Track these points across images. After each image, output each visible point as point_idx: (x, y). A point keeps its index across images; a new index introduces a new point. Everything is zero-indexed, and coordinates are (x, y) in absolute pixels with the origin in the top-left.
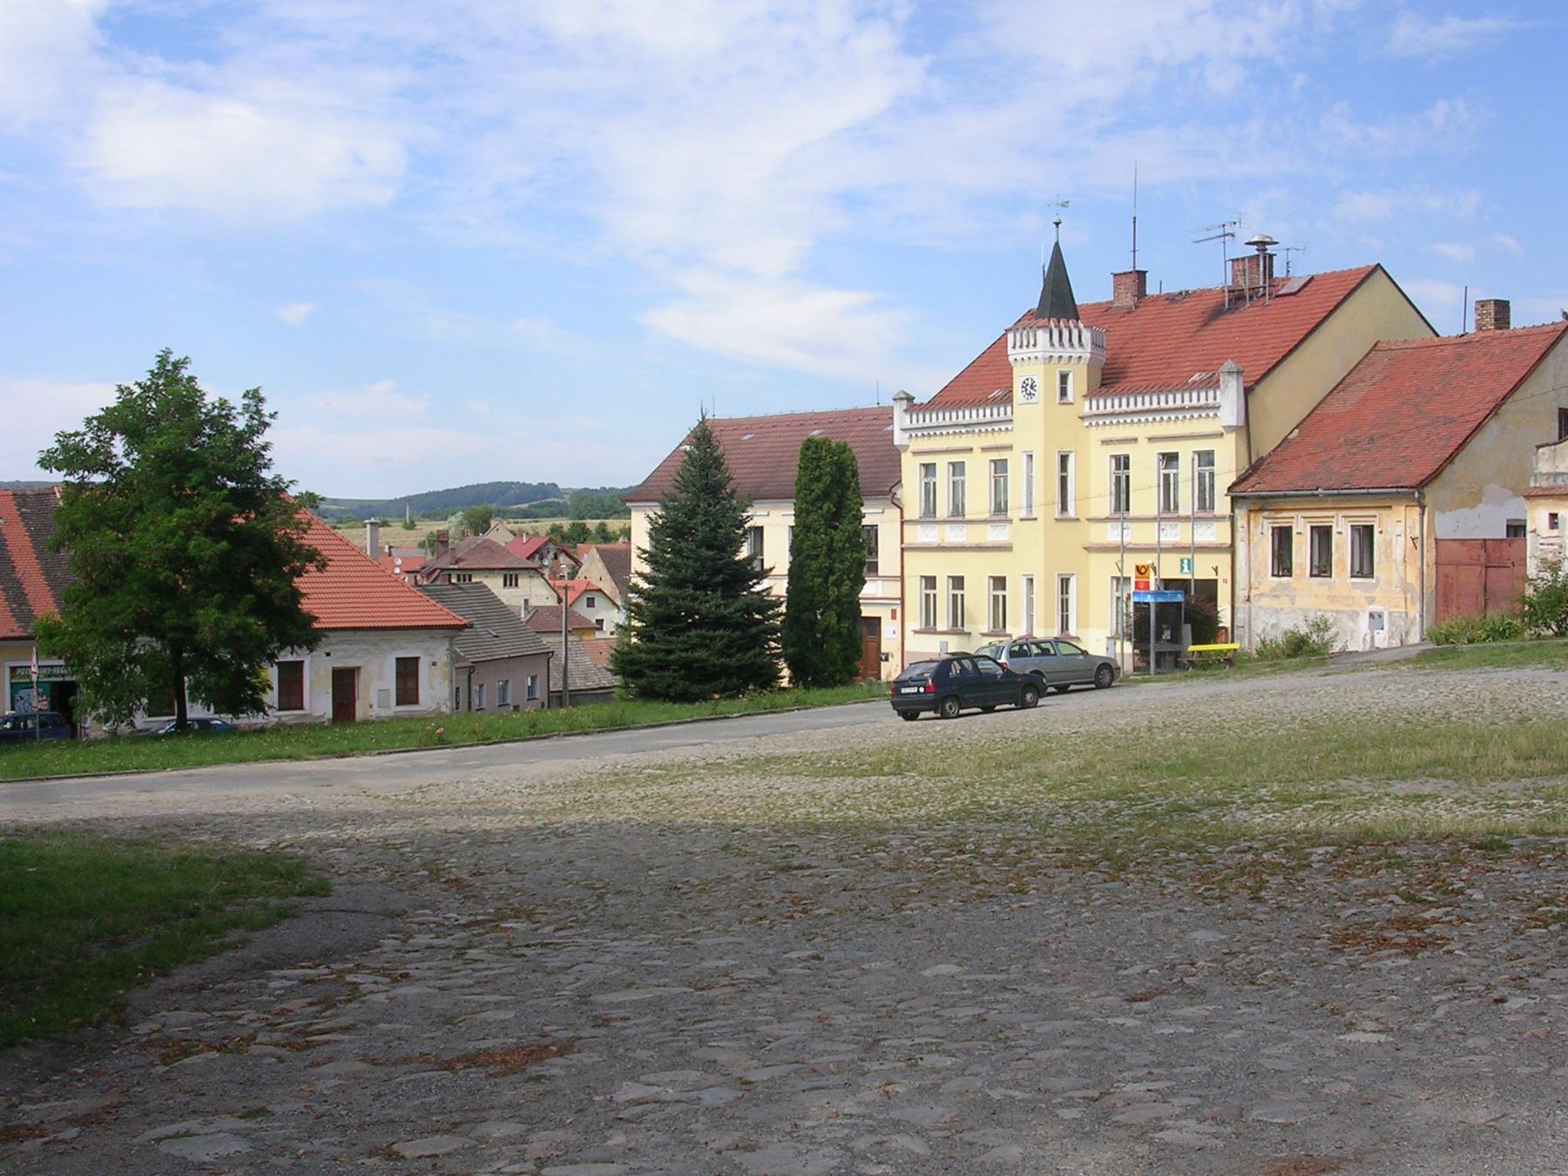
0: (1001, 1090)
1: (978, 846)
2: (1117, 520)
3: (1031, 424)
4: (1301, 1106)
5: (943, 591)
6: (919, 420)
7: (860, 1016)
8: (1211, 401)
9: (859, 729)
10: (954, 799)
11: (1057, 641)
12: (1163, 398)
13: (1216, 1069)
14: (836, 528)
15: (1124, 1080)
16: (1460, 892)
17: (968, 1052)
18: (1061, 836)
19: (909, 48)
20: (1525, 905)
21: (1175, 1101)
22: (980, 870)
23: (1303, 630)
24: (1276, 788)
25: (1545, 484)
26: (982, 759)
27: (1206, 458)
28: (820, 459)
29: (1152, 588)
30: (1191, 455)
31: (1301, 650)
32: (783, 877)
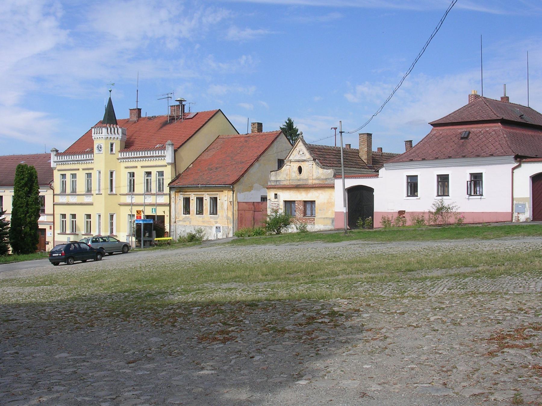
0: (81, 397)
1: (78, 310)
2: (130, 195)
3: (100, 161)
4: (185, 397)
5: (68, 219)
6: (60, 159)
7: (31, 374)
8: (130, 156)
9: (37, 269)
10: (70, 294)
11: (109, 237)
12: (146, 153)
13: (157, 386)
14: (29, 197)
15: (125, 392)
16: (241, 321)
17: (70, 384)
18: (108, 306)
19: (62, 27)
20: (262, 325)
21: (142, 398)
22: (78, 319)
23: (194, 233)
24: (183, 287)
25: (273, 184)
26: (81, 279)
27: (161, 174)
28: (23, 172)
29: (142, 218)
30: (156, 172)
31: (193, 240)
32: (6, 324)
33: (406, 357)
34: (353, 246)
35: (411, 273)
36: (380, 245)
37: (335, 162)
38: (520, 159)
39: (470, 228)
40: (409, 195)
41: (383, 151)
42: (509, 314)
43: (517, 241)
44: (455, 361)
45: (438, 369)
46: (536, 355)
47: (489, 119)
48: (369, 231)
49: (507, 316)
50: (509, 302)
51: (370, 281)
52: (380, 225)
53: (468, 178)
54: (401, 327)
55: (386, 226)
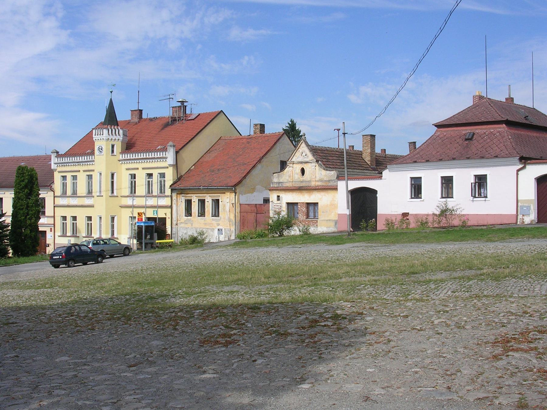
0: (81, 401)
1: (78, 313)
2: (131, 196)
3: (101, 163)
4: (186, 401)
5: (69, 221)
6: (60, 160)
7: (31, 377)
8: (131, 157)
9: (37, 272)
10: (71, 297)
11: (110, 239)
12: (147, 154)
13: (158, 389)
14: (29, 199)
15: (126, 396)
16: (244, 324)
17: (70, 388)
18: (109, 309)
19: (63, 27)
20: (265, 328)
21: (143, 402)
22: (78, 322)
23: (196, 235)
24: (184, 290)
25: (275, 186)
26: (82, 282)
27: (163, 175)
28: (23, 173)
29: (144, 220)
30: (157, 174)
31: (195, 242)
32: (6, 327)
33: (410, 360)
34: (356, 249)
35: (415, 275)
36: (384, 248)
37: (338, 164)
38: (525, 160)
39: (474, 230)
40: (413, 196)
41: (387, 153)
42: (513, 317)
43: (522, 244)
44: (459, 364)
45: (442, 372)
46: (541, 358)
47: (494, 120)
48: (373, 234)
49: (512, 319)
50: (514, 305)
51: (374, 284)
52: (384, 227)
53: (472, 180)
54: (405, 330)
55: (389, 228)
